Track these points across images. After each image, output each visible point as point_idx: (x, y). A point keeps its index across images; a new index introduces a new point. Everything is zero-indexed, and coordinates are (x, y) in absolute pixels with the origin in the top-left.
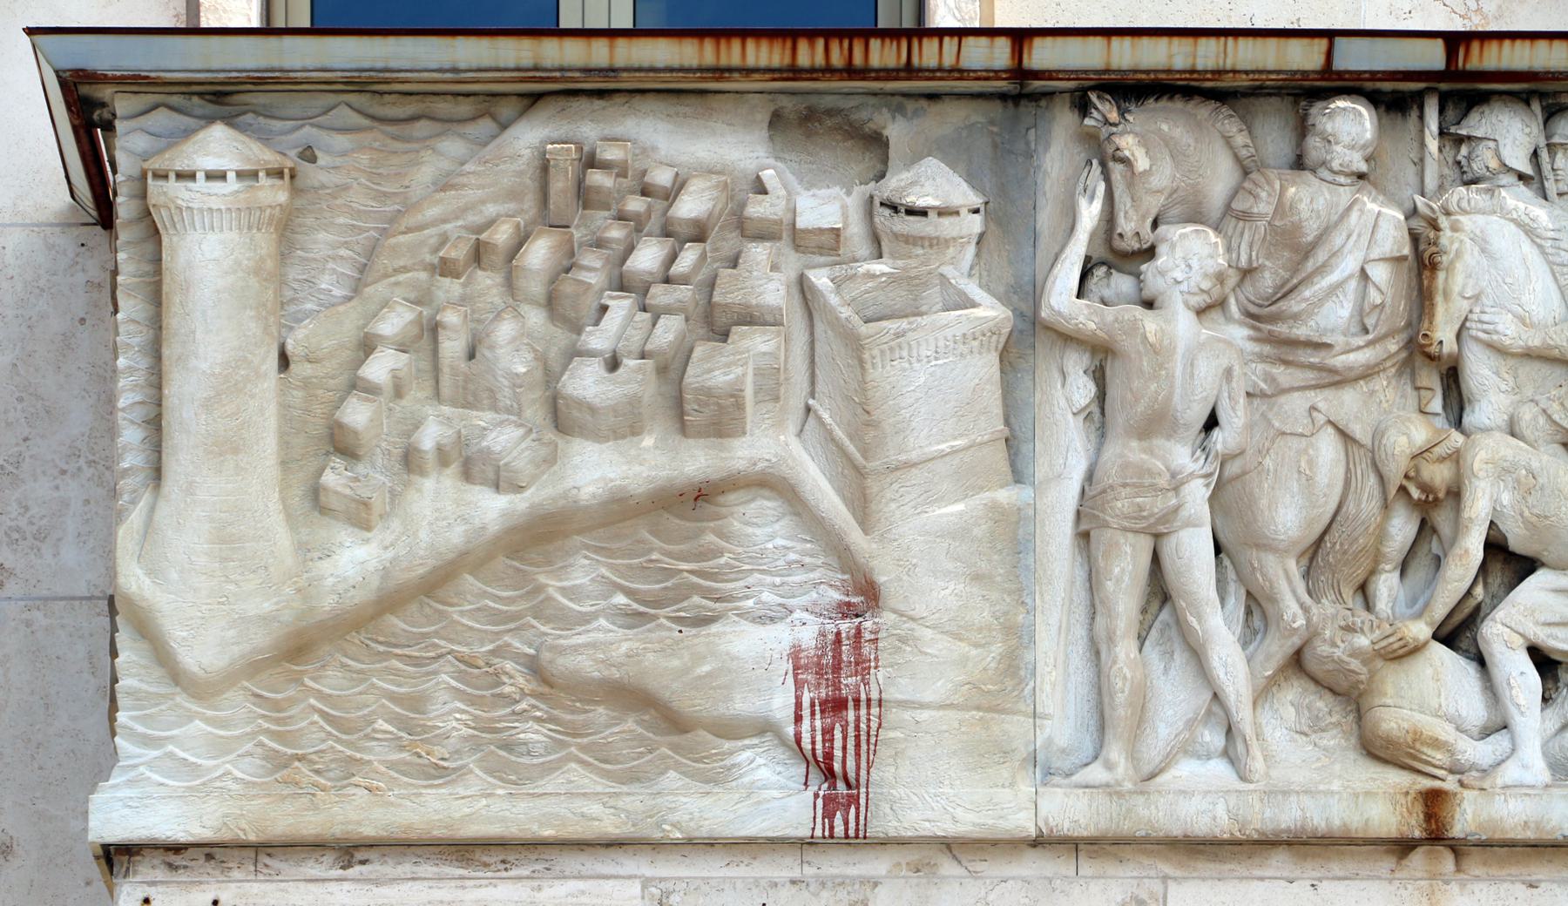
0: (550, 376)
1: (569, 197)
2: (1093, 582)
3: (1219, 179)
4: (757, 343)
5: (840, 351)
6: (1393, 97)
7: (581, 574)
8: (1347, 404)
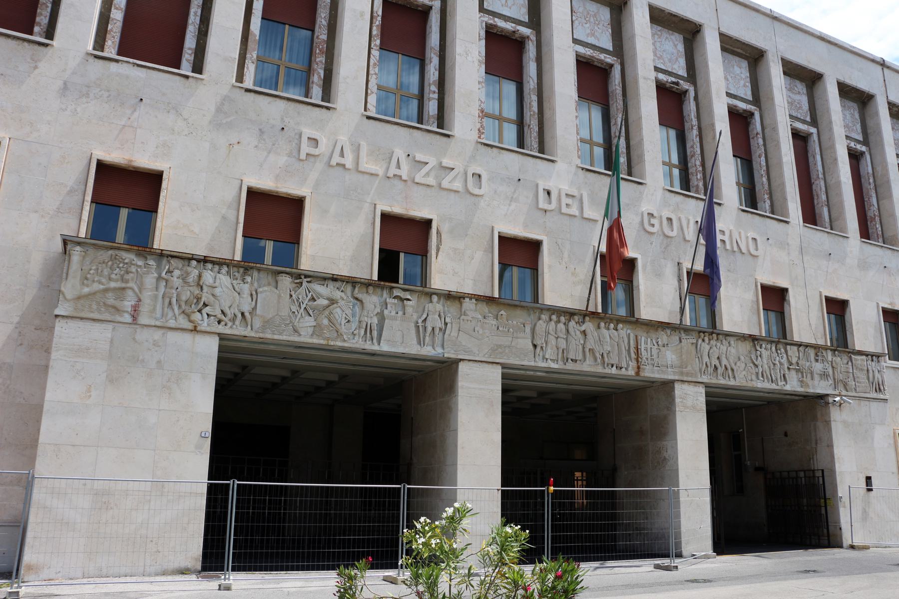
0: (109, 275)
1: (113, 258)
2: (163, 302)
3: (180, 266)
4: (132, 275)
5: (140, 277)
6: (198, 261)
7: (110, 294)
8: (191, 288)
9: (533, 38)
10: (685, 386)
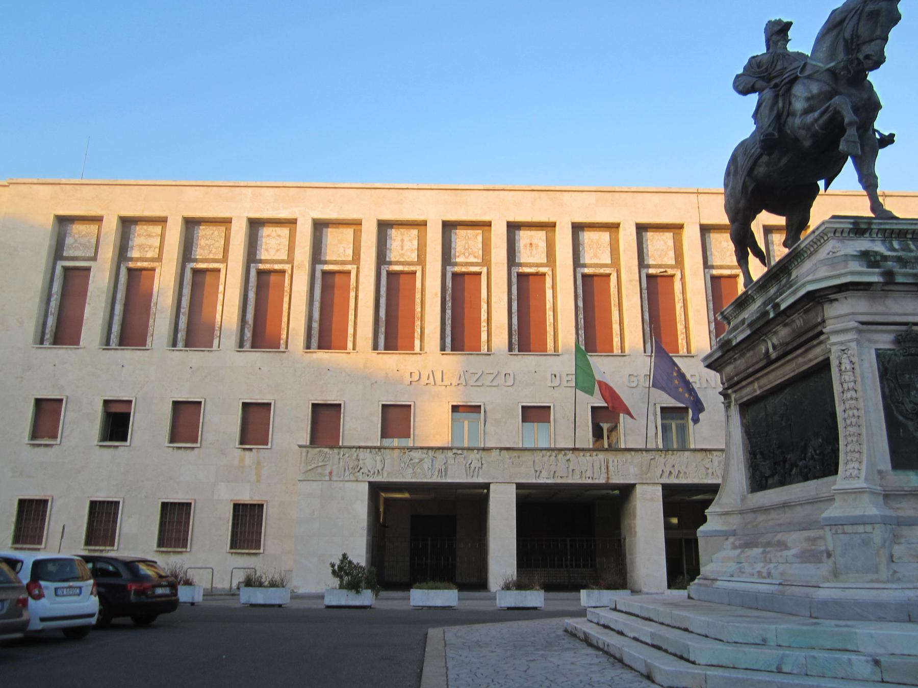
9: (551, 273)
10: (645, 487)
